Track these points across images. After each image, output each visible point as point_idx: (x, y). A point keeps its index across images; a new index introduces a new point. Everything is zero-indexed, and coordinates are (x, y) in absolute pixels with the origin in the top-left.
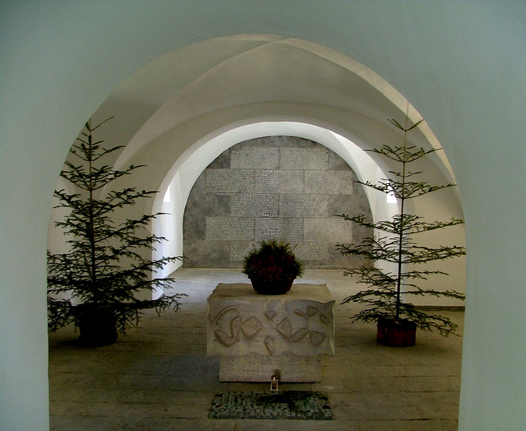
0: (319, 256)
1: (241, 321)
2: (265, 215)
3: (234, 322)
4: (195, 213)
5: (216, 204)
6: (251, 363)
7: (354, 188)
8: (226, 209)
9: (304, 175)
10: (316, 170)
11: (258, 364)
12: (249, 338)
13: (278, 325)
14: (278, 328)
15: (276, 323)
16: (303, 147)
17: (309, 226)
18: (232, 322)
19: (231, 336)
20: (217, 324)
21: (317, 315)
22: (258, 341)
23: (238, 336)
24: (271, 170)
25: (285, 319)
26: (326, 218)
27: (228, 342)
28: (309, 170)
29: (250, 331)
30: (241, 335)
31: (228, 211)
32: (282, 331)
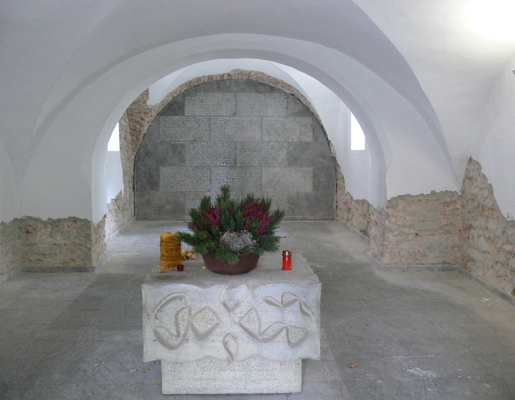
1: (190, 314)
2: (222, 164)
3: (180, 315)
6: (206, 369)
7: (314, 135)
9: (261, 121)
10: (274, 117)
11: (215, 369)
12: (202, 337)
13: (241, 318)
14: (242, 322)
15: (239, 315)
16: (261, 93)
18: (177, 314)
19: (176, 334)
20: (157, 318)
21: (297, 304)
22: (214, 341)
23: (185, 334)
25: (252, 309)
27: (174, 342)
28: (267, 117)
29: (202, 327)
30: (190, 332)
31: (182, 160)
32: (247, 326)
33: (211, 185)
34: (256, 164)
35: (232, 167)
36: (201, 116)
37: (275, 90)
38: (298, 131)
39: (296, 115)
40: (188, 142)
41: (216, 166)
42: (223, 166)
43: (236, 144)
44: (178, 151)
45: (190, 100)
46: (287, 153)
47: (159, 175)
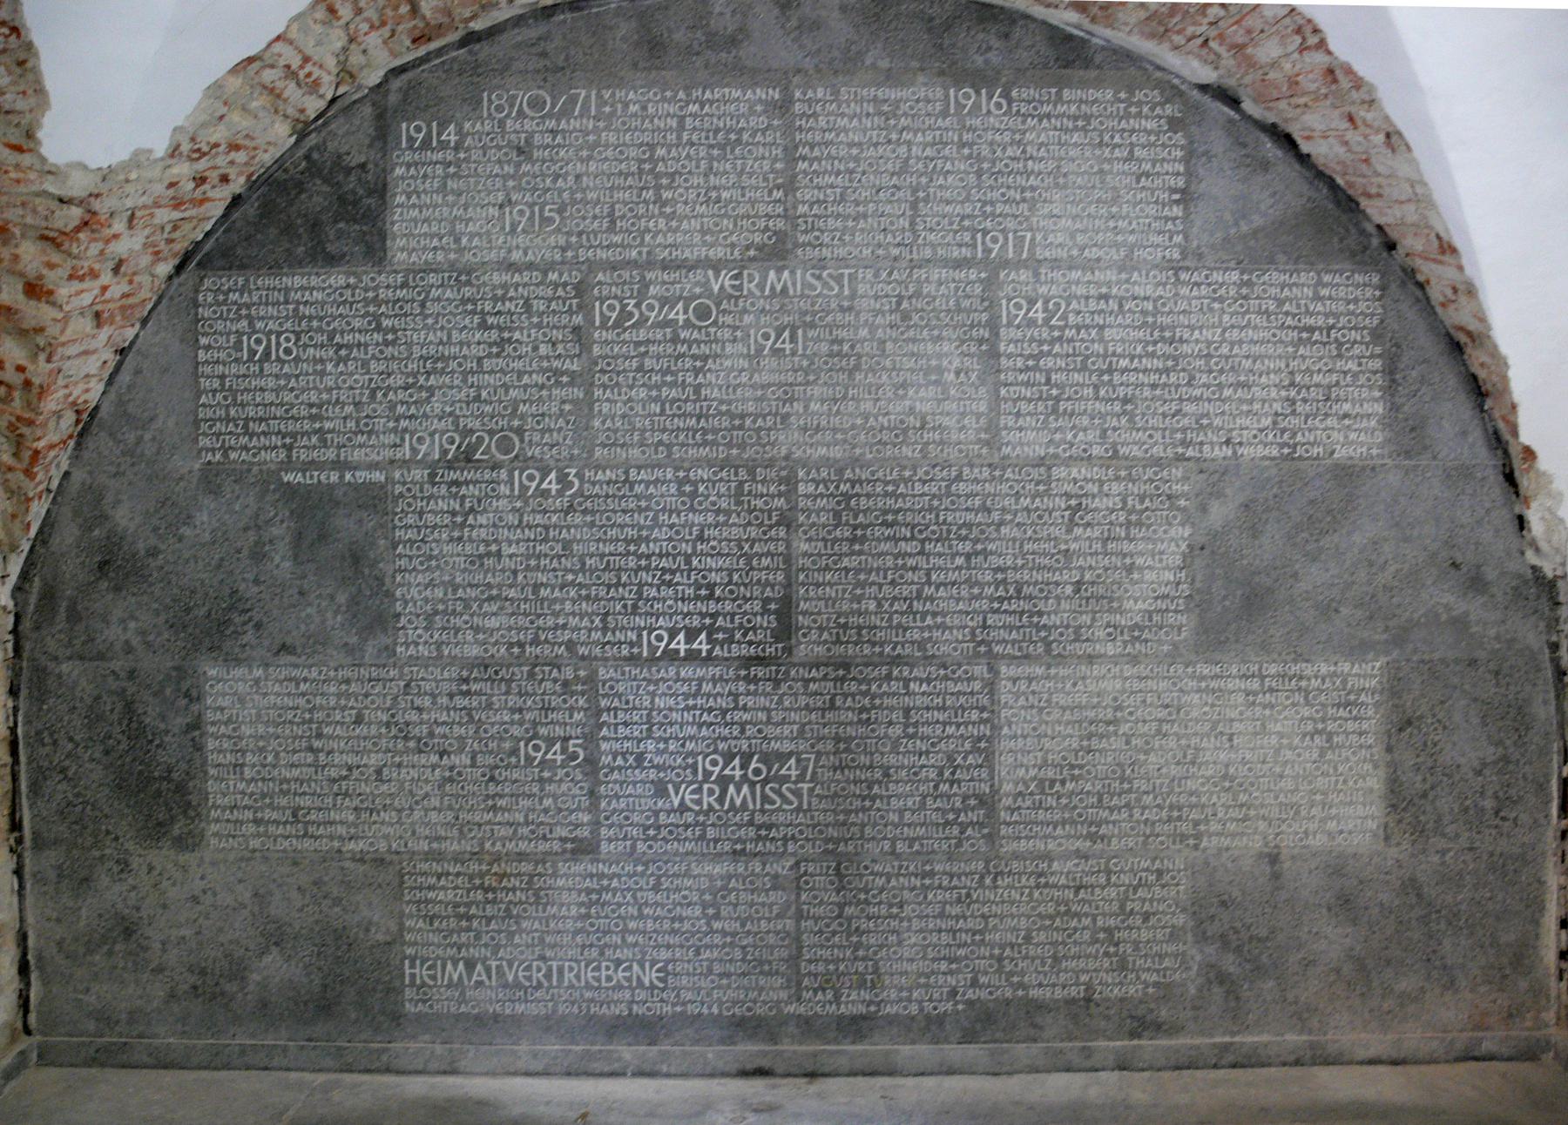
0: (1123, 966)
2: (680, 644)
4: (113, 633)
5: (281, 563)
7: (1395, 408)
8: (354, 601)
9: (991, 305)
10: (1091, 266)
16: (980, 79)
17: (1037, 719)
24: (717, 266)
26: (1173, 657)
31: (374, 615)
33: (594, 808)
34: (949, 643)
35: (760, 660)
36: (512, 267)
37: (1087, 63)
38: (1275, 371)
39: (1255, 252)
40: (419, 474)
41: (633, 659)
42: (692, 656)
43: (790, 482)
44: (336, 539)
45: (426, 144)
46: (1195, 549)
47: (196, 725)
